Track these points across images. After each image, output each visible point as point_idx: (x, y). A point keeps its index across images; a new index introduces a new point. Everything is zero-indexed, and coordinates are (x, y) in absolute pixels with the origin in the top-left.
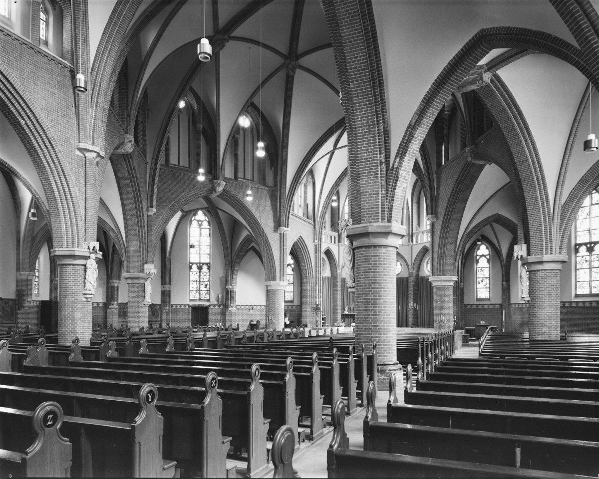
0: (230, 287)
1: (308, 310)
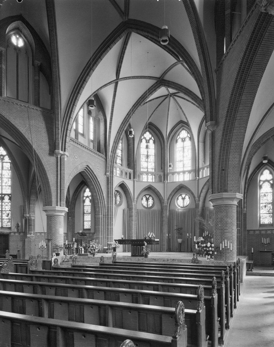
0: (28, 215)
1: (100, 236)
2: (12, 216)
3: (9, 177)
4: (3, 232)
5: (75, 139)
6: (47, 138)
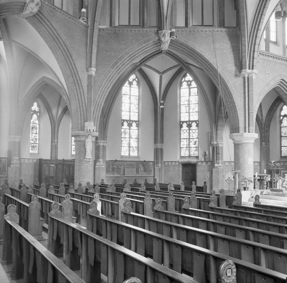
0: (215, 143)
2: (199, 144)
3: (196, 102)
4: (190, 161)
5: (266, 52)
6: (233, 58)
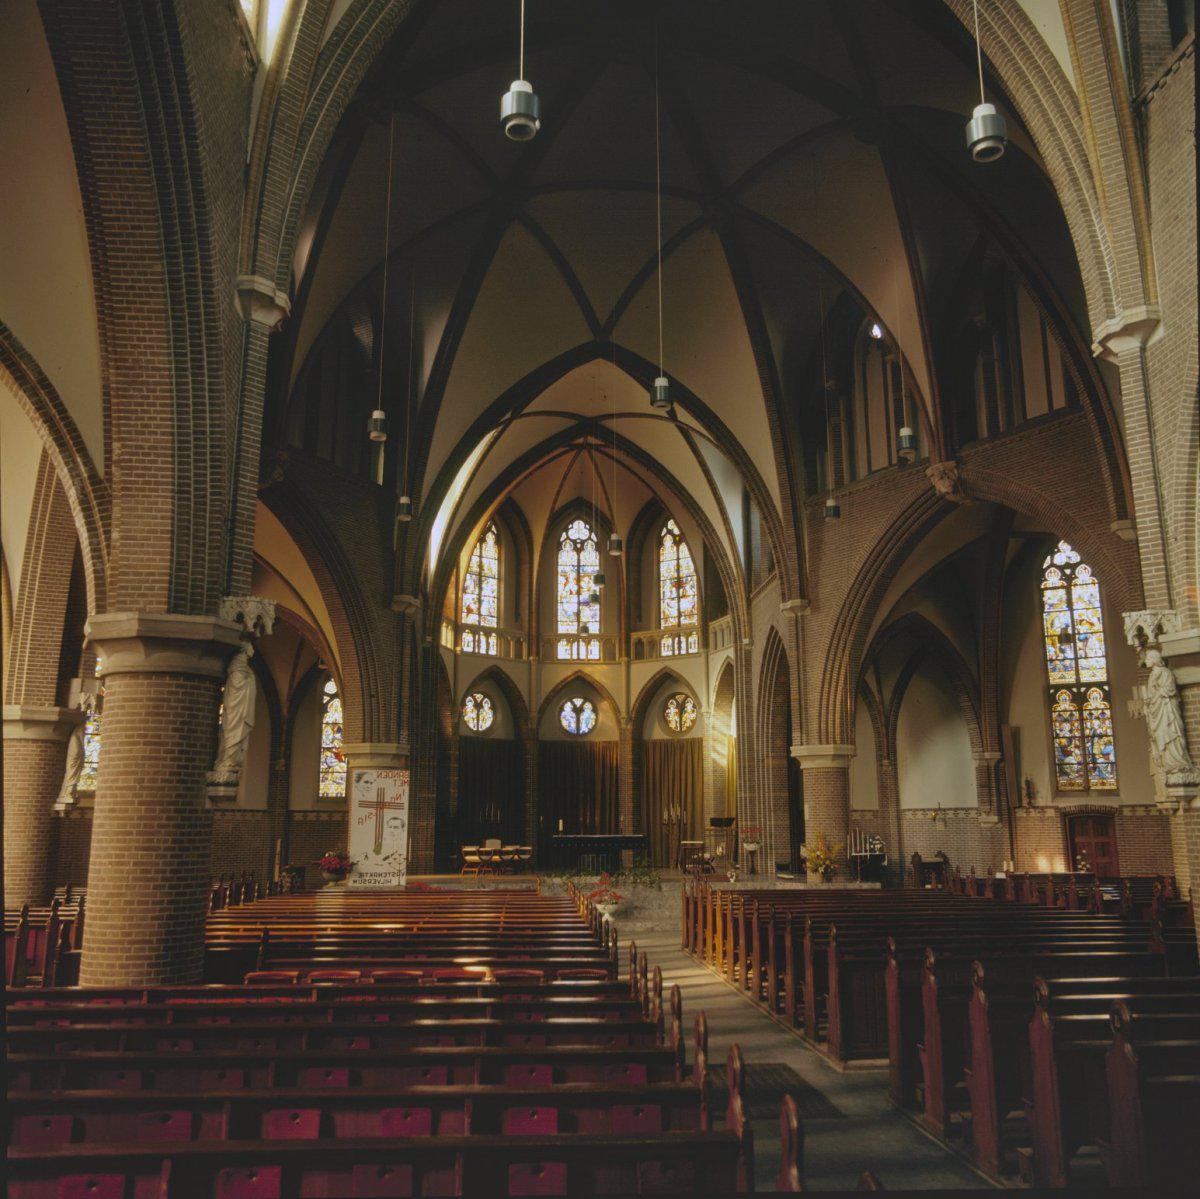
0: (987, 755)
